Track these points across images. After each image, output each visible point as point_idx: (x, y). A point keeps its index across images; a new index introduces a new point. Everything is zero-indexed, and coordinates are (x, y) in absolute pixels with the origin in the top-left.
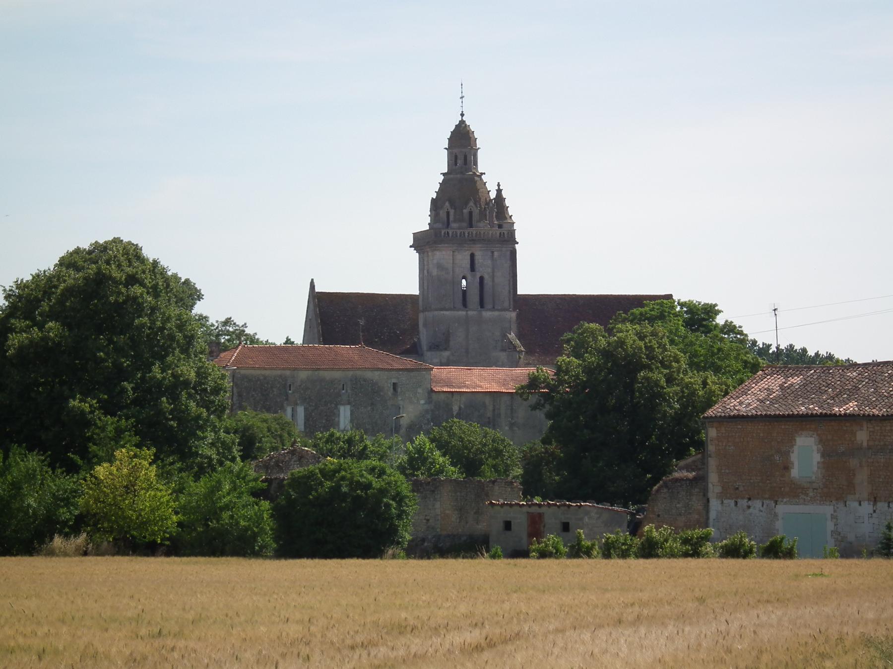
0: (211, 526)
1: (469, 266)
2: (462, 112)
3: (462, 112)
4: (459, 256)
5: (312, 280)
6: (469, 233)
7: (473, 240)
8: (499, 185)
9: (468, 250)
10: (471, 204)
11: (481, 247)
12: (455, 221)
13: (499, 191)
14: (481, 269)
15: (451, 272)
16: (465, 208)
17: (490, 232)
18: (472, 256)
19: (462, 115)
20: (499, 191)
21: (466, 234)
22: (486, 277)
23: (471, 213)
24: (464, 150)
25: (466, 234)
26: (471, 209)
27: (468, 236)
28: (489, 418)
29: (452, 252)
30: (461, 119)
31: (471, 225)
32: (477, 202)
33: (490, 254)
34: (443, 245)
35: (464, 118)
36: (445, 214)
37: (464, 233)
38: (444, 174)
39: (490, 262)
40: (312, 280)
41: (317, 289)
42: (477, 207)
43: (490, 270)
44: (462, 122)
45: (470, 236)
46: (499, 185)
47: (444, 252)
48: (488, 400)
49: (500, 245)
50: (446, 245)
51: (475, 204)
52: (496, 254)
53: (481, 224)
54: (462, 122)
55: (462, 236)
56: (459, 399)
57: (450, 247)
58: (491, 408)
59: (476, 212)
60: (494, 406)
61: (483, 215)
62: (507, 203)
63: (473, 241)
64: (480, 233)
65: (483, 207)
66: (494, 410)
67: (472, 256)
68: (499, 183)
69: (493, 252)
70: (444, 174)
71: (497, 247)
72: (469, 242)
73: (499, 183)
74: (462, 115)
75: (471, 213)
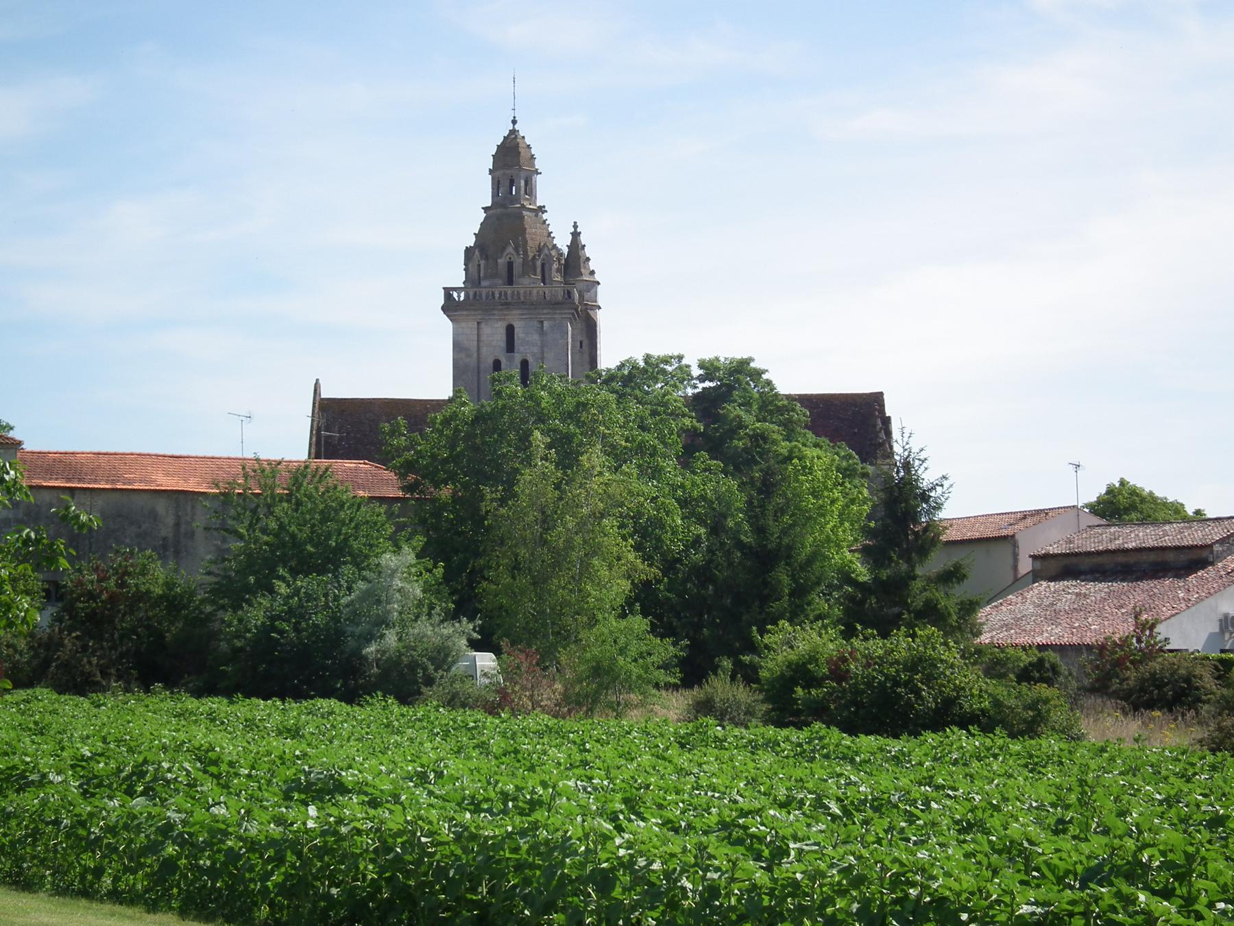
0: (620, 822)
1: (503, 344)
2: (514, 117)
3: (514, 117)
4: (486, 330)
5: (317, 380)
6: (500, 294)
7: (506, 304)
8: (575, 226)
9: (500, 320)
10: (510, 249)
11: (522, 314)
12: (486, 278)
13: (576, 235)
14: (522, 349)
15: (475, 355)
16: (501, 257)
17: (535, 291)
18: (510, 330)
19: (514, 122)
20: (576, 235)
21: (497, 295)
22: (530, 360)
23: (510, 265)
24: (508, 172)
25: (497, 295)
26: (510, 258)
27: (500, 298)
28: (164, 539)
29: (476, 323)
30: (511, 128)
31: (510, 281)
32: (521, 246)
33: (536, 324)
34: (460, 313)
35: (517, 127)
36: (476, 267)
37: (493, 294)
38: (486, 209)
39: (536, 337)
40: (317, 380)
41: (325, 394)
42: (518, 254)
43: (536, 350)
44: (513, 132)
45: (503, 297)
46: (575, 226)
47: (463, 324)
48: (161, 506)
49: (551, 311)
50: (465, 313)
51: (516, 250)
52: (546, 324)
53: (526, 281)
54: (513, 132)
55: (491, 297)
56: (89, 503)
57: (473, 315)
58: (170, 521)
59: (518, 261)
60: (178, 517)
61: (529, 266)
62: (588, 252)
63: (507, 305)
64: (518, 293)
65: (531, 255)
66: (177, 525)
67: (510, 330)
68: (575, 223)
69: (542, 322)
70: (486, 209)
71: (565, 313)
72: (500, 307)
73: (575, 223)
74: (514, 122)
75: (510, 265)
